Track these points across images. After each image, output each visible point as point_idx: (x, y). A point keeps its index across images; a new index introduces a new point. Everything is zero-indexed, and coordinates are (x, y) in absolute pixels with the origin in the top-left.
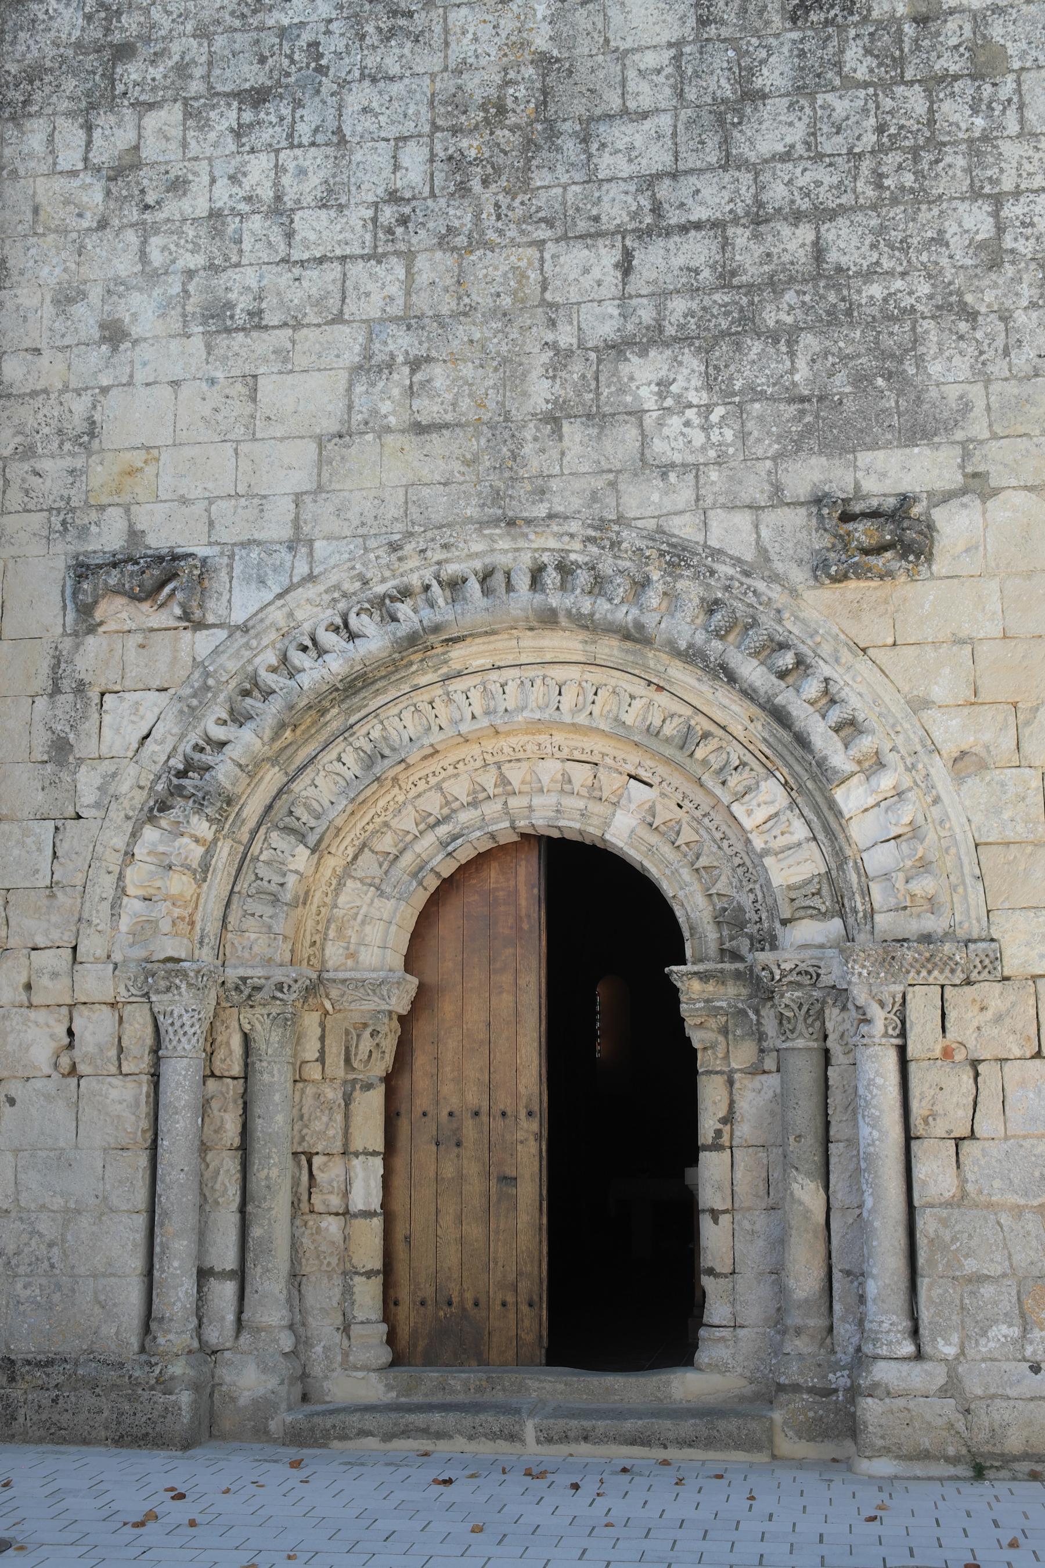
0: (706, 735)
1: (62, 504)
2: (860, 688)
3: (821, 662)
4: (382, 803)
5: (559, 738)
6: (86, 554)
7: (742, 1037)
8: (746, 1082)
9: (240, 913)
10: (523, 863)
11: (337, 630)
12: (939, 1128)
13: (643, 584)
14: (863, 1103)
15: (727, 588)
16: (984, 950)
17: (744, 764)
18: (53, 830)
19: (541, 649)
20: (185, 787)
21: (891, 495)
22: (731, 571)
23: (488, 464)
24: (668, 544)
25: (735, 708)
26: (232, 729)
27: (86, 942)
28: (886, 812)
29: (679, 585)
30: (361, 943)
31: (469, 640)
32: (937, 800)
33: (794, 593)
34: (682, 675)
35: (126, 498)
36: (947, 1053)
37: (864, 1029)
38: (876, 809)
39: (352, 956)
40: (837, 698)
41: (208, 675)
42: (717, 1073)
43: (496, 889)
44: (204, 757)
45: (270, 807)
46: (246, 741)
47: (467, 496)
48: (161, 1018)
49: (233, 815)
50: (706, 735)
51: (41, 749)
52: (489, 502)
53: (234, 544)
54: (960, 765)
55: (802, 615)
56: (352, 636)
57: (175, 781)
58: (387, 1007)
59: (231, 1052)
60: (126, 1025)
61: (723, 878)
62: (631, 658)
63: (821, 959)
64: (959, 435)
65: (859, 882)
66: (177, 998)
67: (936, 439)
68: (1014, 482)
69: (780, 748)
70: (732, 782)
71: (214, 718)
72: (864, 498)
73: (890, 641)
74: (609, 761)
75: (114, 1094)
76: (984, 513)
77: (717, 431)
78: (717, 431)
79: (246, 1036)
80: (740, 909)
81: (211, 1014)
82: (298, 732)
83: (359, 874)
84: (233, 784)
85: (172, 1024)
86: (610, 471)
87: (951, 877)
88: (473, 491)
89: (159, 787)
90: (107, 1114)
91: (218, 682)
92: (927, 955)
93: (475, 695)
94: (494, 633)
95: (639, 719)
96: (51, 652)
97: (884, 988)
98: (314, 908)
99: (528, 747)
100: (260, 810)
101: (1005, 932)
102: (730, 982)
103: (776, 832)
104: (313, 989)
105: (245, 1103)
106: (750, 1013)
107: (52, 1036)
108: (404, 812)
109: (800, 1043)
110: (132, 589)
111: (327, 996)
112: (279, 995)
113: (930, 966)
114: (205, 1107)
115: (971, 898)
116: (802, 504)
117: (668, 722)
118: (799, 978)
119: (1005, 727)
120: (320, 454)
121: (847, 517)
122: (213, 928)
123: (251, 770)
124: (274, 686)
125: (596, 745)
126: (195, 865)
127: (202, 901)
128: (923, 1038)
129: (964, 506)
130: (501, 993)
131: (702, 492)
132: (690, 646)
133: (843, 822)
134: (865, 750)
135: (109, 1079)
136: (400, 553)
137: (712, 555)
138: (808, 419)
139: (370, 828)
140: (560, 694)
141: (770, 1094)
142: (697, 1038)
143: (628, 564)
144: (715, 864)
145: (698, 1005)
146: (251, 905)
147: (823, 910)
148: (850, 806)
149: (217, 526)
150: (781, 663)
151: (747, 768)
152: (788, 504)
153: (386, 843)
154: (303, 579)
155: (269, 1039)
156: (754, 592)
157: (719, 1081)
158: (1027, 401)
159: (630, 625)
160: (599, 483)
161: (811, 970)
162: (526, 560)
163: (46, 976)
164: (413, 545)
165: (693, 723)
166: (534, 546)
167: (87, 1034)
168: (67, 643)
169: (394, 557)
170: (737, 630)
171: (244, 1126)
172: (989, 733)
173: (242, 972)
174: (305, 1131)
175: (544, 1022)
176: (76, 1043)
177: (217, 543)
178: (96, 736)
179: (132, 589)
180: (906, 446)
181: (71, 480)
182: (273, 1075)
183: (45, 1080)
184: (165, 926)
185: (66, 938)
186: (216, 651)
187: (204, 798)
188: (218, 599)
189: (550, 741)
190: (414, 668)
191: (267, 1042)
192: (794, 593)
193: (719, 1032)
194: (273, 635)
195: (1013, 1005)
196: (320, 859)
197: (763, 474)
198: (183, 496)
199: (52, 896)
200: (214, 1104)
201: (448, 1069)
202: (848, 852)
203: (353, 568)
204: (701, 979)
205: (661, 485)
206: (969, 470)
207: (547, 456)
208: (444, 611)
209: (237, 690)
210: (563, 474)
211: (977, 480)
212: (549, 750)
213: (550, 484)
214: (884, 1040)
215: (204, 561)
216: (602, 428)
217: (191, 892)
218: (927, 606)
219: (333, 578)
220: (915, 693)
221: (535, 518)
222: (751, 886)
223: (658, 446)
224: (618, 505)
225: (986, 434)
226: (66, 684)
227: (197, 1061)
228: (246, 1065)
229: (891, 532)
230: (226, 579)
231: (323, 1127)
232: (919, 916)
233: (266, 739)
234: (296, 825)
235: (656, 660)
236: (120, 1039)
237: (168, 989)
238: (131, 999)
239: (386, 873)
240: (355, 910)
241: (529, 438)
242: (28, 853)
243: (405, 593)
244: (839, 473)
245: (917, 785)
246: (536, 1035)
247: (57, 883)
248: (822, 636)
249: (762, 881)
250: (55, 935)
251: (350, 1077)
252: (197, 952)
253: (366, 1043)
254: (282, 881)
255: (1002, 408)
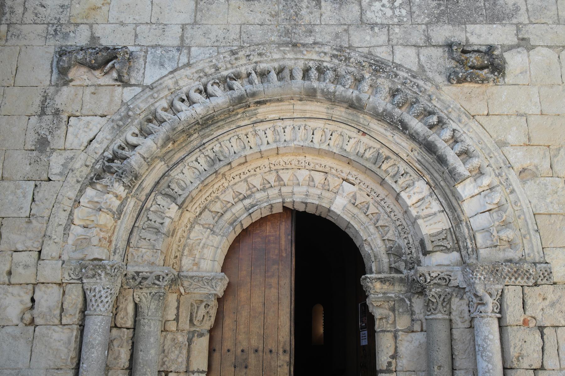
0: (387, 158)
1: (55, 22)
2: (470, 137)
3: (451, 122)
4: (216, 186)
5: (309, 158)
6: (66, 46)
7: (403, 313)
8: (403, 337)
9: (138, 237)
10: (284, 223)
11: (200, 92)
12: (525, 364)
13: (359, 80)
14: (481, 349)
15: (404, 84)
16: (544, 268)
17: (407, 173)
18: (33, 186)
19: (305, 111)
20: (112, 167)
21: (483, 45)
22: (406, 75)
23: (283, 17)
24: (374, 60)
25: (404, 144)
26: (141, 139)
27: (47, 248)
28: (485, 197)
29: (379, 81)
30: (202, 258)
31: (268, 104)
32: (512, 192)
33: (437, 87)
34: (376, 126)
35: (91, 21)
36: (525, 323)
37: (482, 308)
38: (479, 196)
39: (197, 264)
40: (459, 140)
41: (129, 109)
42: (388, 331)
43: (270, 236)
44: (124, 152)
45: (158, 183)
46: (148, 145)
47: (272, 31)
48: (88, 292)
49: (138, 185)
50: (387, 158)
51: (31, 143)
52: (283, 35)
53: (148, 46)
54: (523, 175)
55: (442, 98)
56: (209, 96)
57: (107, 164)
58: (215, 292)
59: (127, 313)
60: (66, 296)
61: (391, 232)
62: (351, 117)
63: (452, 272)
64: (514, 21)
65: (469, 233)
66: (98, 281)
67: (504, 22)
68: (542, 44)
69: (427, 165)
70: (400, 181)
71: (131, 132)
72: (471, 45)
73: (486, 113)
74: (334, 171)
75: (56, 336)
76: (529, 56)
77: (398, 10)
78: (398, 10)
79: (136, 304)
80: (400, 247)
81: (118, 292)
82: (176, 144)
83: (202, 222)
84: (139, 168)
85: (95, 296)
86: (345, 24)
87: (522, 231)
88: (275, 29)
89: (97, 167)
90: (50, 348)
91: (135, 114)
92: (515, 269)
93: (269, 133)
94: (280, 100)
95: (353, 149)
96: (42, 94)
97: (493, 287)
98: (177, 239)
99: (293, 162)
100: (152, 184)
101: (552, 259)
102: (397, 284)
103: (423, 207)
104: (176, 280)
105: (133, 343)
106: (407, 300)
107: (21, 302)
108: (227, 192)
109: (439, 316)
110: (90, 61)
111: (182, 285)
112: (157, 282)
113: (516, 275)
114: (110, 345)
115: (534, 241)
116: (440, 46)
117: (368, 151)
118: (440, 281)
119: (545, 156)
120: (196, 6)
121: (464, 52)
122: (122, 244)
123: (150, 161)
124: (165, 118)
125: (328, 162)
126: (114, 209)
127: (117, 230)
128: (514, 313)
129: (519, 52)
130: (270, 288)
131: (391, 37)
132: (385, 110)
133: (460, 202)
134: (474, 165)
135: (54, 327)
136: (236, 56)
137: (396, 67)
138: (442, 8)
139: (209, 199)
140: (313, 134)
141: (417, 343)
142: (378, 313)
143: (353, 69)
144: (387, 224)
145: (379, 296)
146: (144, 234)
147: (449, 247)
148: (466, 194)
149: (139, 37)
150: (431, 121)
151: (408, 175)
152: (434, 46)
153: (217, 207)
154: (184, 65)
155: (149, 307)
156: (418, 86)
157: (390, 336)
158: (545, 8)
159: (354, 99)
160: (340, 29)
161: (446, 277)
162: (301, 64)
163: (21, 267)
164: (243, 52)
165: (381, 151)
166: (306, 57)
167: (42, 301)
168: (52, 90)
169: (233, 57)
170: (406, 105)
171: (132, 355)
172: (535, 159)
173: (137, 269)
174: (165, 359)
175: (293, 304)
176: (36, 306)
177: (139, 45)
178: (64, 138)
179: (90, 61)
180: (490, 24)
181: (61, 10)
182: (151, 327)
183: (14, 328)
184: (95, 241)
185: (35, 245)
186: (135, 98)
187: (122, 174)
188: (137, 72)
189: (306, 160)
190: (239, 116)
191: (149, 309)
192: (437, 87)
193: (390, 310)
194: (166, 92)
195: (560, 297)
196: (182, 213)
197: (421, 31)
198: (122, 22)
199: (30, 222)
200: (116, 343)
201: (242, 327)
202: (463, 218)
203: (211, 61)
204: (381, 282)
205: (371, 32)
206: (520, 36)
207: (313, 15)
208: (257, 85)
209: (145, 119)
210: (321, 24)
211: (524, 42)
212: (303, 164)
213: (314, 28)
214: (493, 314)
215: (131, 53)
216: (341, 5)
217: (111, 224)
218: (503, 97)
219: (201, 66)
220: (500, 138)
221: (307, 44)
222: (406, 236)
223: (369, 15)
224: (349, 40)
225: (527, 22)
226: (49, 111)
227: (107, 318)
228: (135, 321)
229: (487, 60)
230: (143, 63)
231: (175, 357)
232: (504, 250)
233: (159, 145)
234: (171, 192)
235: (364, 119)
236: (62, 304)
237: (94, 276)
238: (71, 281)
239: (216, 222)
240: (199, 241)
241: (304, 6)
242: (16, 199)
243: (237, 77)
244: (458, 33)
245: (502, 184)
246: (288, 310)
247: (33, 215)
248: (452, 109)
249: (412, 233)
250: (29, 244)
251: (192, 329)
252: (112, 257)
253: (202, 311)
254: (162, 222)
255: (534, 11)
